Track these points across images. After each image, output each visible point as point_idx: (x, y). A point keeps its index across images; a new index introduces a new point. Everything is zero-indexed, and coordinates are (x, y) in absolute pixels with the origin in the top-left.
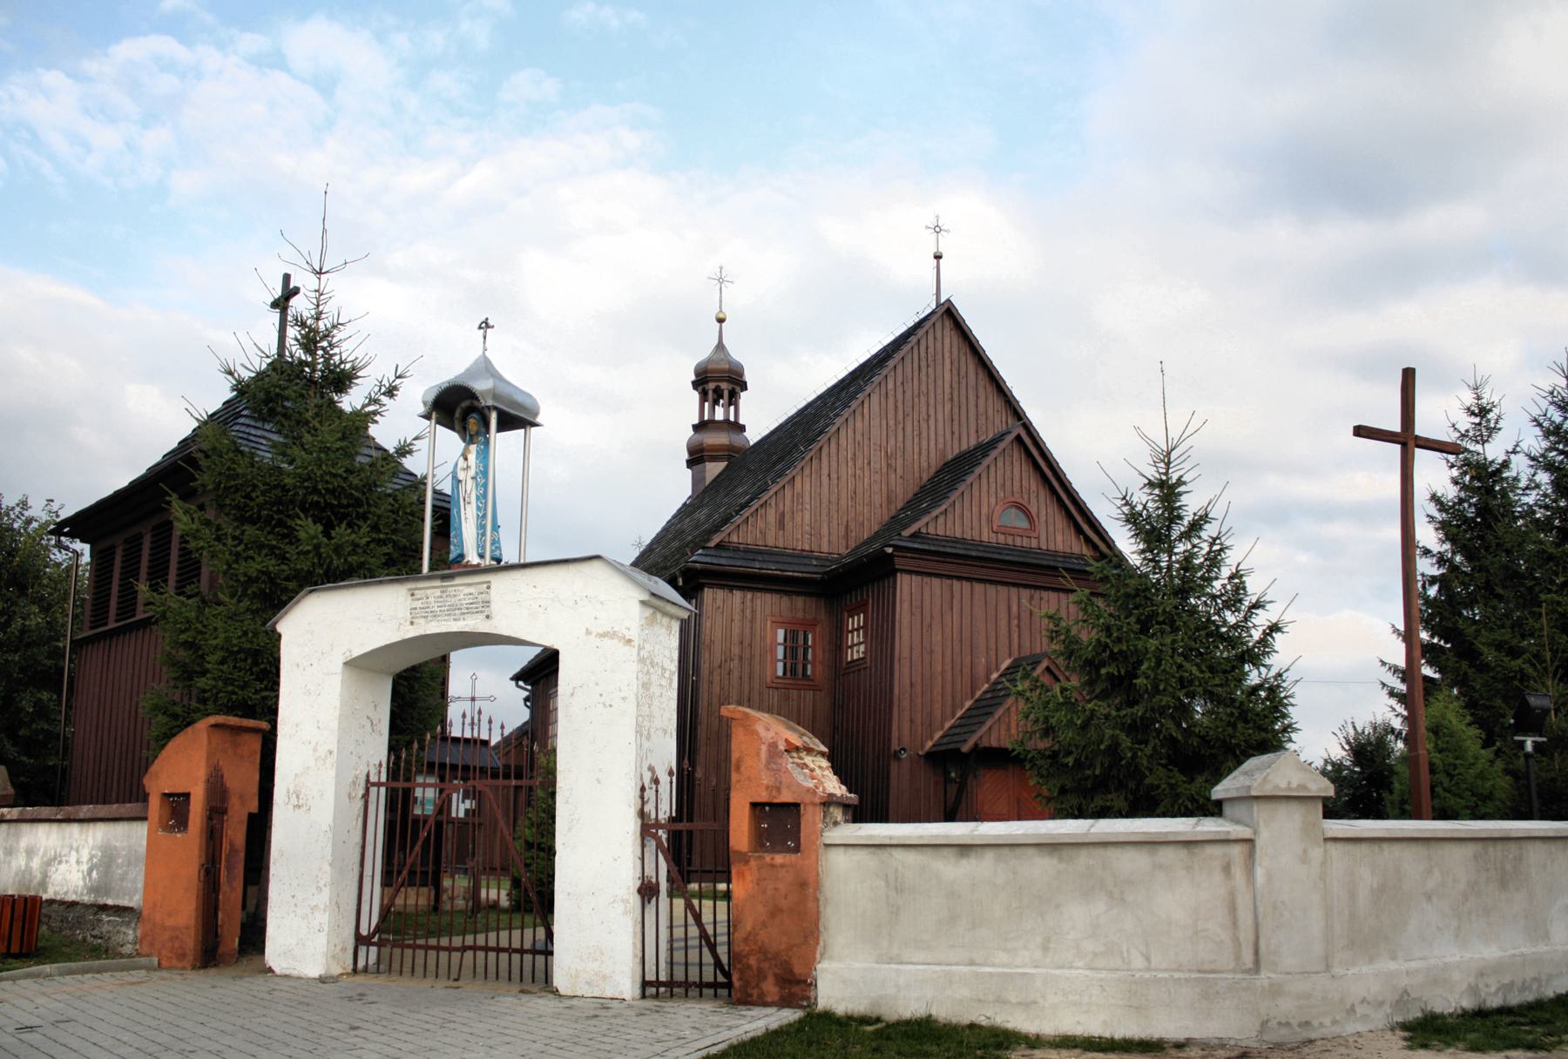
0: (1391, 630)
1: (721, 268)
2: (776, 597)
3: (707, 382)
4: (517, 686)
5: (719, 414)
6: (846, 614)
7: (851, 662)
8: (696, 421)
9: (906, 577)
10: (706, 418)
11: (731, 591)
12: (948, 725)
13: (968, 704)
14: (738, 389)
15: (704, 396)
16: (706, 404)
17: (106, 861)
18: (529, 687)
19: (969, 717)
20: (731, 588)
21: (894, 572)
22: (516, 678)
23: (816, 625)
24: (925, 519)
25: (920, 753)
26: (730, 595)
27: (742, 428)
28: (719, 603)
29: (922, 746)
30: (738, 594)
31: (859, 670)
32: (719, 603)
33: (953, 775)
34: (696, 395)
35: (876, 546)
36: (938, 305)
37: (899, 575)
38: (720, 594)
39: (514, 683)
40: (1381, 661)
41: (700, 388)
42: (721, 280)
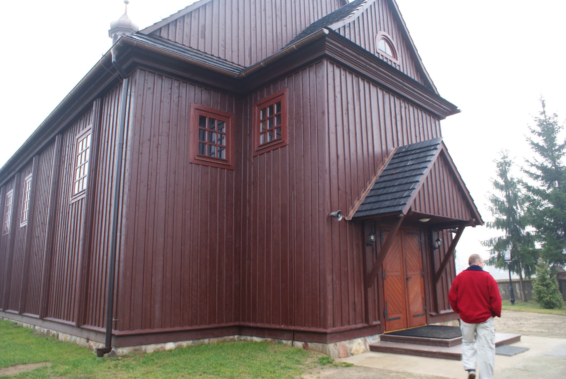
3: (118, 31)
6: (257, 108)
21: (318, 61)
41: (113, 35)
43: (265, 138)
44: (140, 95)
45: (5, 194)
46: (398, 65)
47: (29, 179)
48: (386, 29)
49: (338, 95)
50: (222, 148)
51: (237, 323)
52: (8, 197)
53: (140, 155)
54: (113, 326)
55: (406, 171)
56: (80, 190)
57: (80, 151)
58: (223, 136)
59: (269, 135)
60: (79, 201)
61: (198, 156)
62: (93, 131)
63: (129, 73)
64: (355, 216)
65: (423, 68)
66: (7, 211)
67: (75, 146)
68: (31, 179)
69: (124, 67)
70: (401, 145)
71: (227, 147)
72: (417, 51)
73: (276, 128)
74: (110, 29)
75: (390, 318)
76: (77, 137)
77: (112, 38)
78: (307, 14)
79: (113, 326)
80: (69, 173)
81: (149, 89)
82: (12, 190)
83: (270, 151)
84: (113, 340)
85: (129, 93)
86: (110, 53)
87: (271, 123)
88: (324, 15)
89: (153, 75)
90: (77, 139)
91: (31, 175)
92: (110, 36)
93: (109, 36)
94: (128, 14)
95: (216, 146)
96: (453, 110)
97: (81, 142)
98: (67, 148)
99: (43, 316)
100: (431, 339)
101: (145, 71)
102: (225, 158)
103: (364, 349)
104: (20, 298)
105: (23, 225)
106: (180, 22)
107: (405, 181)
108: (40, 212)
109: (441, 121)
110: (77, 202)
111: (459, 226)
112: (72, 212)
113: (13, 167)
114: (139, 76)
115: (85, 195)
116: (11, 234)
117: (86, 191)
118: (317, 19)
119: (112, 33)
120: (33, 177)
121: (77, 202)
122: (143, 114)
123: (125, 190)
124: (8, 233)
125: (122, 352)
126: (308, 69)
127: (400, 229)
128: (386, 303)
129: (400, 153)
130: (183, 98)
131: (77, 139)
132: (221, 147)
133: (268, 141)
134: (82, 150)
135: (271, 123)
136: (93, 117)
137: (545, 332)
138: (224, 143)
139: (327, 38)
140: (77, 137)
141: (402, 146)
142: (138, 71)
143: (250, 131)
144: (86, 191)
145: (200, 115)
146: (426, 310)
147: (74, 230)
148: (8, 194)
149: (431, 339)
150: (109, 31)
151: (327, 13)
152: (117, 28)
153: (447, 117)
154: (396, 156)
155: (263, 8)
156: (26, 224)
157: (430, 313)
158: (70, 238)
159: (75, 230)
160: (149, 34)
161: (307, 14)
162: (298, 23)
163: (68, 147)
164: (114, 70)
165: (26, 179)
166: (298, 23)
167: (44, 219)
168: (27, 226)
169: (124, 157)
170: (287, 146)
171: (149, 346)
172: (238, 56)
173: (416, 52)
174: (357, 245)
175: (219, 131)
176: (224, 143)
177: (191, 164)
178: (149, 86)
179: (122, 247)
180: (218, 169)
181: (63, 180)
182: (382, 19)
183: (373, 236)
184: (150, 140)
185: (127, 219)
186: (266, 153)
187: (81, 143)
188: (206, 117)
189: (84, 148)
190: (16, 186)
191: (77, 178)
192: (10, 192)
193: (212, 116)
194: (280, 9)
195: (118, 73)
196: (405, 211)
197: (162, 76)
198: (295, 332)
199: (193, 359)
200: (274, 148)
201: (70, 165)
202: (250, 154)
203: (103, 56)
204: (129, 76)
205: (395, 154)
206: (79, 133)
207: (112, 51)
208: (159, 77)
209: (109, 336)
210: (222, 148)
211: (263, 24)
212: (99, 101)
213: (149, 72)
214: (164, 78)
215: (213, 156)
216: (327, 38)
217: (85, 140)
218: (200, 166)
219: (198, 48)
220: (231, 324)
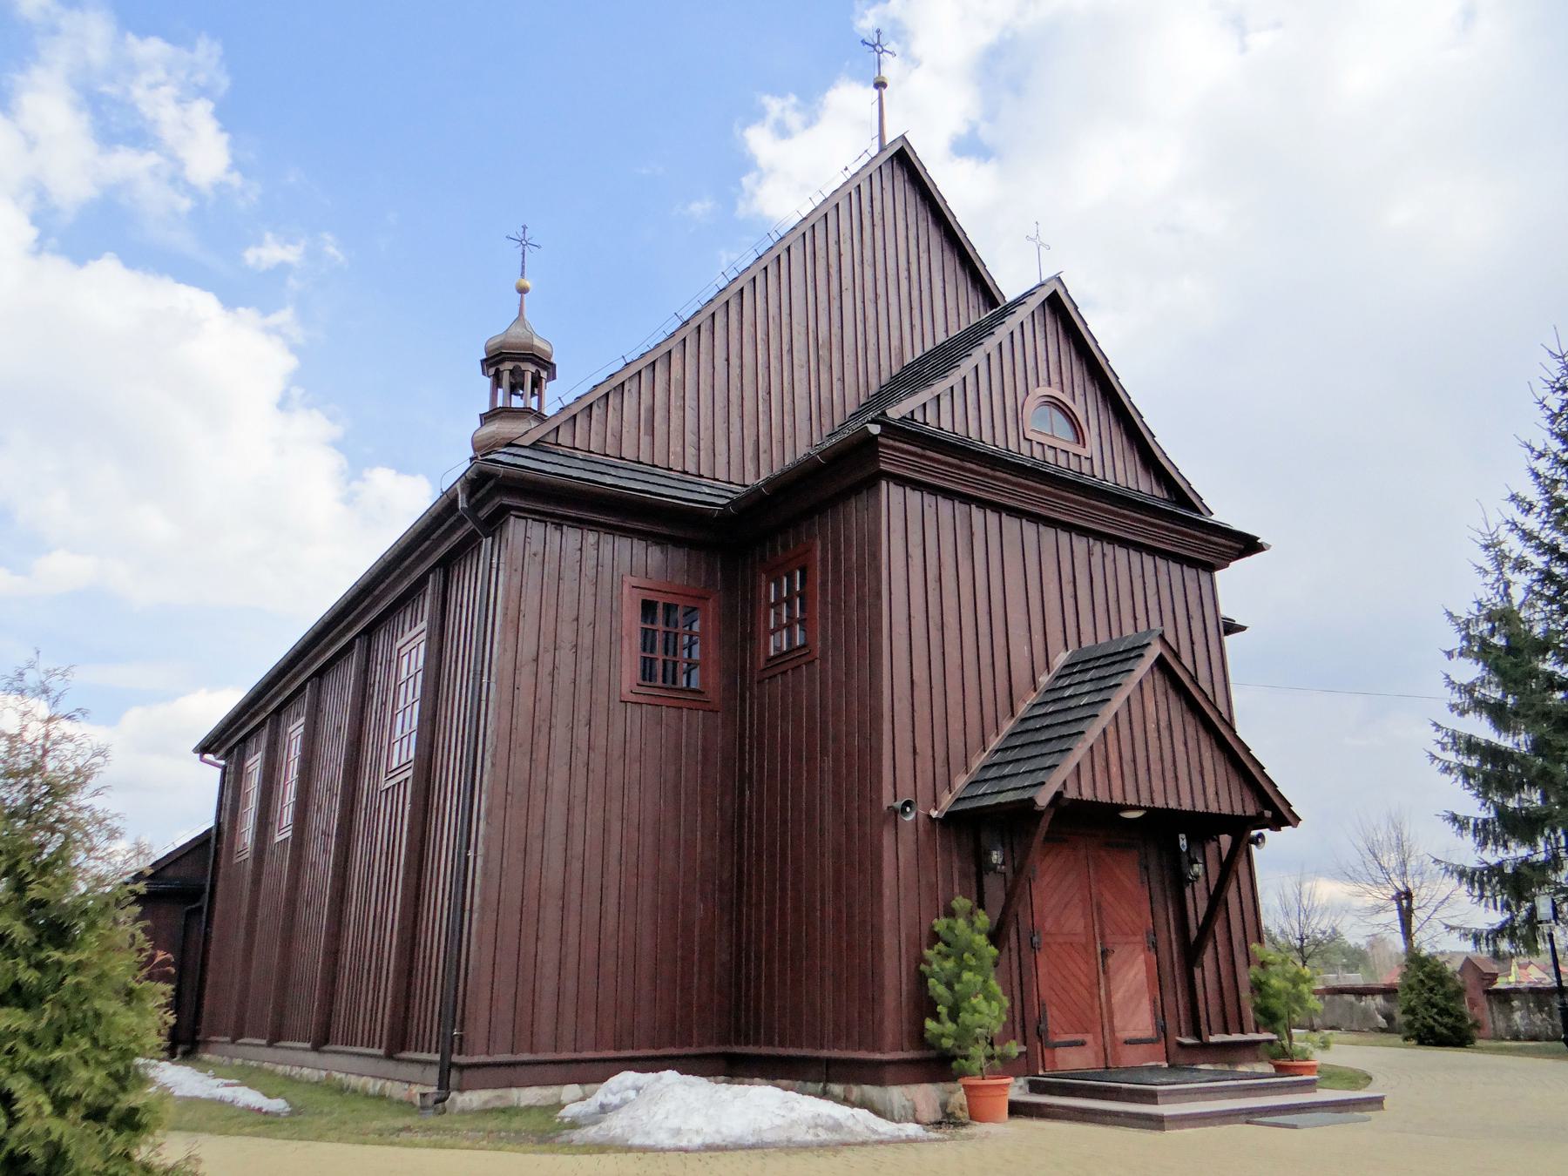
0: (1443, 683)
1: (525, 228)
2: (639, 546)
3: (502, 361)
4: (202, 760)
6: (764, 576)
7: (774, 658)
8: (486, 409)
9: (896, 492)
10: (500, 404)
11: (559, 526)
12: (976, 763)
13: (1008, 726)
14: (544, 374)
16: (500, 391)
17: (1544, 905)
18: (222, 762)
19: (1006, 749)
20: (560, 522)
21: (871, 482)
22: (204, 748)
23: (708, 599)
24: (925, 396)
25: (934, 814)
26: (558, 534)
28: (536, 546)
29: (935, 803)
30: (572, 536)
31: (785, 672)
32: (536, 546)
33: (996, 857)
34: (487, 382)
35: (855, 426)
36: (882, 149)
37: (884, 483)
38: (536, 530)
39: (197, 756)
40: (1435, 724)
41: (492, 371)
42: (524, 243)
43: (791, 639)
44: (516, 570)
45: (243, 765)
46: (1086, 458)
47: (295, 730)
48: (1055, 378)
49: (916, 553)
50: (691, 665)
51: (721, 1049)
52: (250, 770)
53: (516, 691)
54: (456, 1046)
55: (1070, 709)
56: (404, 760)
57: (404, 676)
58: (694, 638)
60: (399, 783)
61: (638, 685)
62: (429, 638)
63: (494, 524)
64: (953, 809)
65: (1158, 453)
66: (246, 805)
67: (391, 663)
68: (301, 729)
69: (484, 513)
70: (1087, 641)
71: (702, 664)
72: (1141, 417)
74: (484, 357)
75: (1057, 1040)
76: (399, 645)
78: (895, 342)
79: (456, 1046)
80: (381, 722)
81: (535, 555)
82: (259, 755)
83: (799, 666)
84: (454, 1076)
85: (495, 566)
86: (456, 489)
88: (941, 338)
90: (399, 650)
91: (302, 720)
93: (484, 374)
96: (1248, 545)
97: (407, 656)
98: (379, 667)
99: (321, 1041)
100: (1123, 1085)
101: (525, 518)
105: (283, 837)
106: (599, 407)
107: (1064, 731)
108: (319, 808)
109: (1218, 574)
110: (403, 784)
111: (1242, 831)
112: (385, 807)
113: (262, 702)
114: (515, 529)
115: (409, 773)
116: (254, 858)
117: (412, 763)
118: (921, 349)
119: (490, 366)
120: (306, 725)
121: (403, 784)
122: (522, 608)
123: (485, 764)
124: (247, 856)
125: (471, 1100)
126: (865, 492)
127: (1047, 839)
128: (1044, 1005)
129: (1077, 664)
130: (605, 568)
131: (399, 650)
132: (689, 664)
134: (408, 673)
135: (791, 607)
136: (428, 604)
138: (696, 655)
139: (880, 439)
140: (399, 645)
141: (1092, 643)
142: (512, 518)
143: (752, 625)
144: (412, 763)
146: (1164, 1029)
147: (388, 847)
148: (249, 763)
149: (1123, 1085)
150: (483, 362)
151: (947, 331)
153: (1232, 564)
154: (1067, 671)
155: (786, 348)
156: (290, 833)
157: (1179, 1039)
158: (379, 867)
159: (391, 845)
160: (534, 444)
161: (895, 342)
162: (872, 366)
163: (381, 664)
164: (461, 521)
165: (290, 730)
166: (872, 366)
167: (328, 823)
168: (290, 841)
169: (484, 698)
170: (818, 662)
171: (527, 1089)
172: (729, 463)
173: (1137, 420)
174: (964, 875)
175: (687, 628)
176: (696, 655)
177: (623, 704)
178: (534, 549)
179: (477, 882)
181: (369, 740)
184: (536, 660)
185: (487, 823)
186: (779, 677)
187: (406, 659)
189: (413, 671)
190: (268, 747)
191: (398, 734)
192: (254, 758)
193: (670, 599)
194: (827, 345)
195: (469, 525)
196: (1043, 798)
197: (562, 525)
198: (830, 1062)
200: (794, 664)
201: (384, 704)
202: (752, 677)
203: (443, 493)
204: (494, 531)
205: (1066, 667)
206: (402, 636)
207: (458, 485)
208: (556, 529)
209: (446, 1069)
210: (692, 666)
211: (785, 384)
212: (440, 572)
213: (534, 520)
214: (565, 528)
216: (880, 439)
217: (414, 651)
218: (644, 706)
219: (638, 457)
220: (708, 1049)
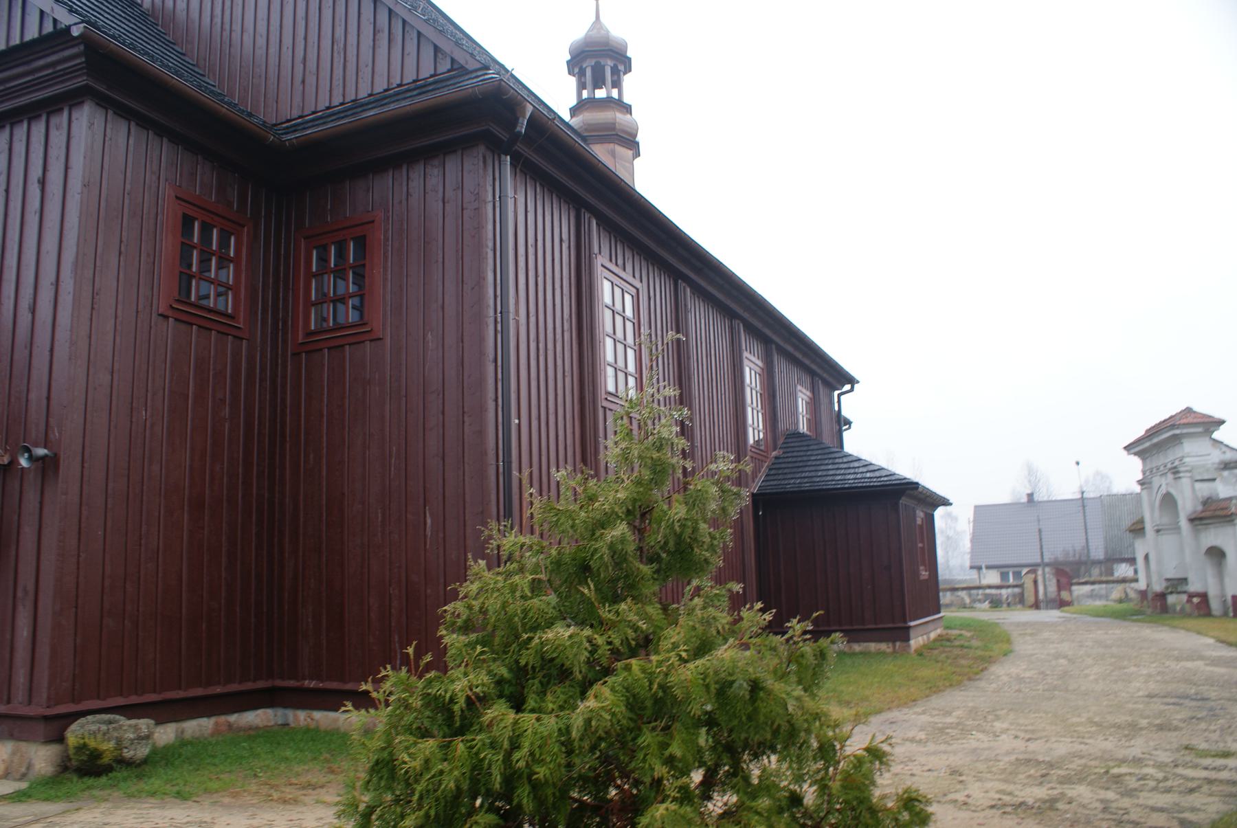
5: (601, 94)
14: (621, 68)
15: (580, 75)
27: (627, 109)
41: (576, 70)
59: (354, 283)
73: (352, 267)
74: (569, 57)
77: (574, 76)
87: (341, 255)
89: (104, 111)
92: (571, 72)
94: (602, 19)
95: (212, 283)
102: (212, 305)
103: (506, 708)
104: (310, 620)
133: (351, 291)
137: (1214, 802)
145: (184, 213)
150: (568, 62)
152: (583, 52)
180: (213, 332)
182: (304, 15)
183: (922, 578)
188: (194, 219)
199: (493, 745)
215: (204, 302)
